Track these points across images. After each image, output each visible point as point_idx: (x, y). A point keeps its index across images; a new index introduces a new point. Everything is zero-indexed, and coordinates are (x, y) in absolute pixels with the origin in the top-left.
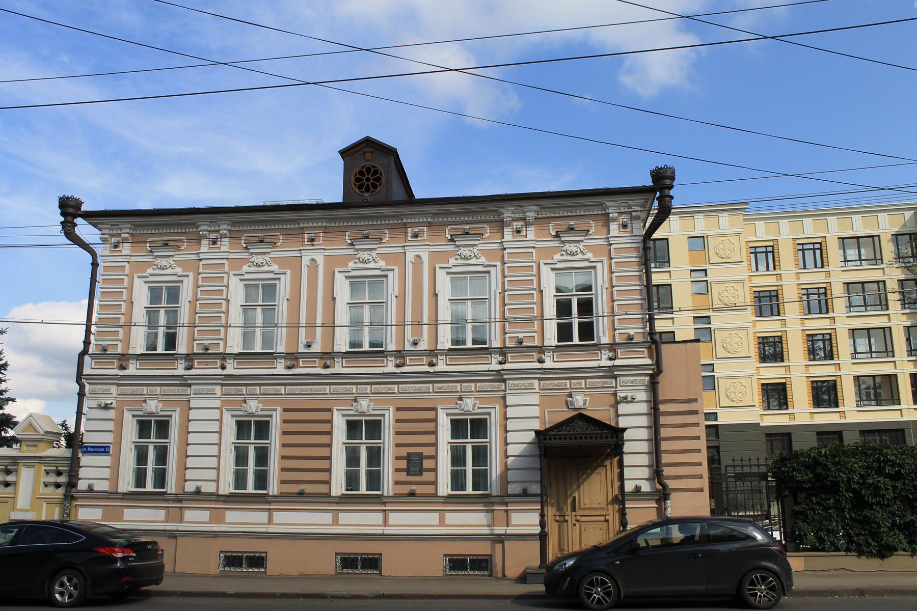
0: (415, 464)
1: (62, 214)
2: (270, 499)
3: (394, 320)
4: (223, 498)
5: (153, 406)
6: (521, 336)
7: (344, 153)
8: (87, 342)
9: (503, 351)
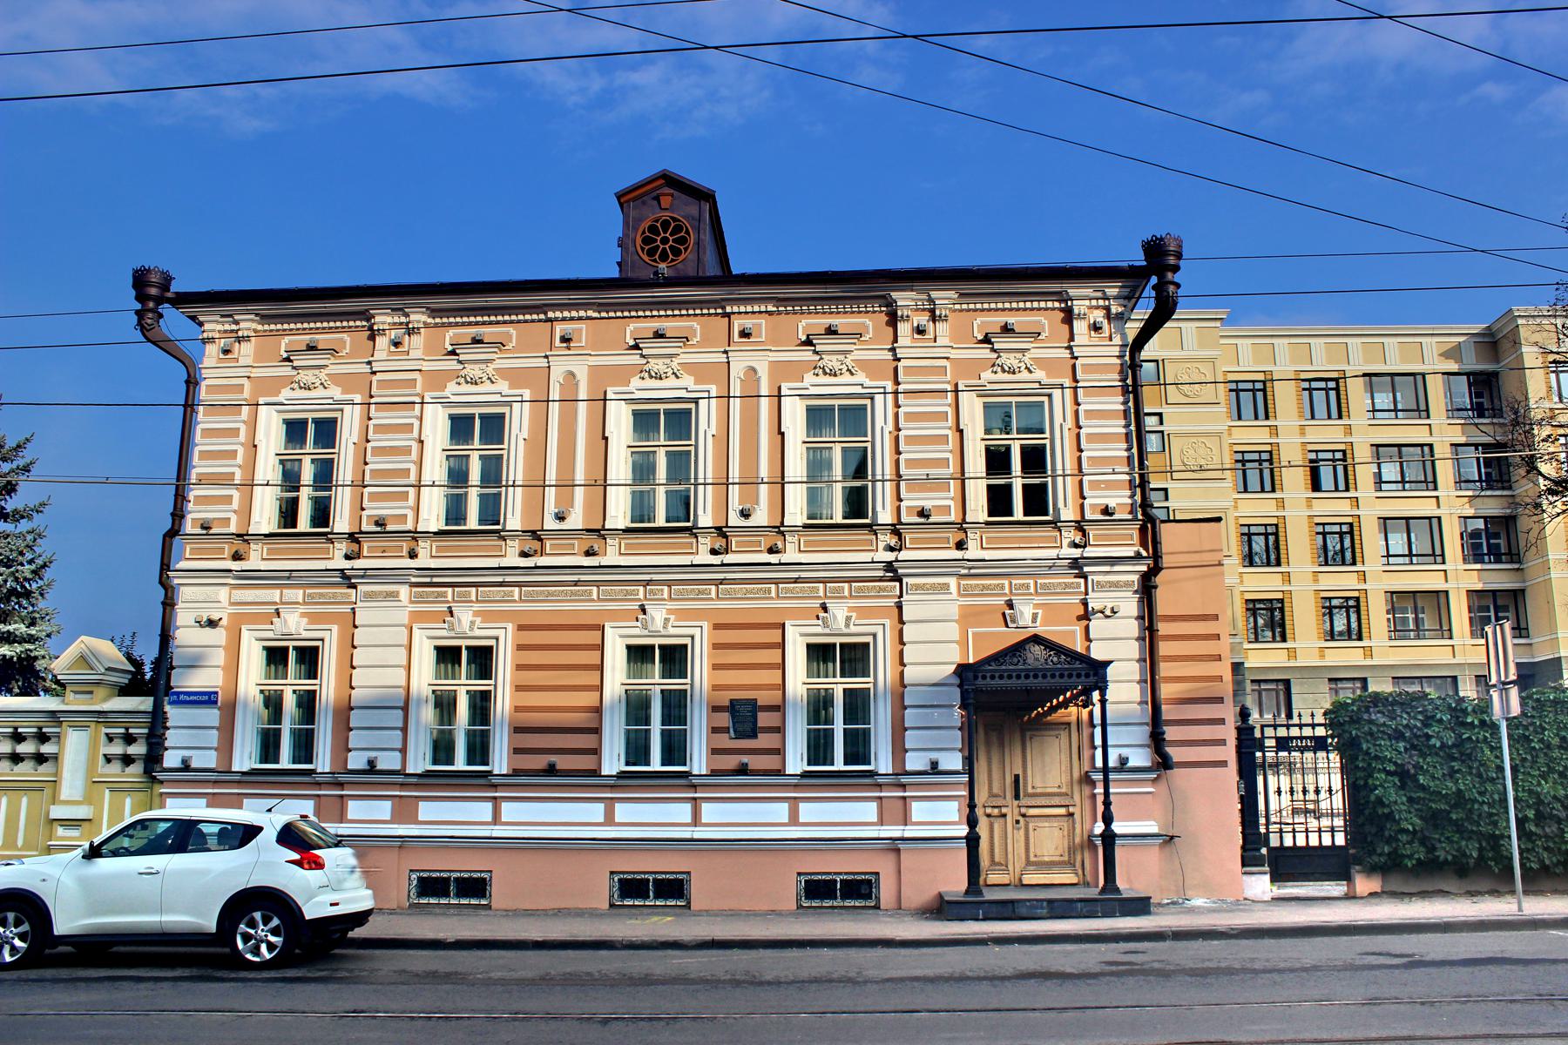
1: (138, 298)
2: (495, 781)
3: (710, 474)
4: (414, 780)
6: (928, 504)
7: (625, 198)
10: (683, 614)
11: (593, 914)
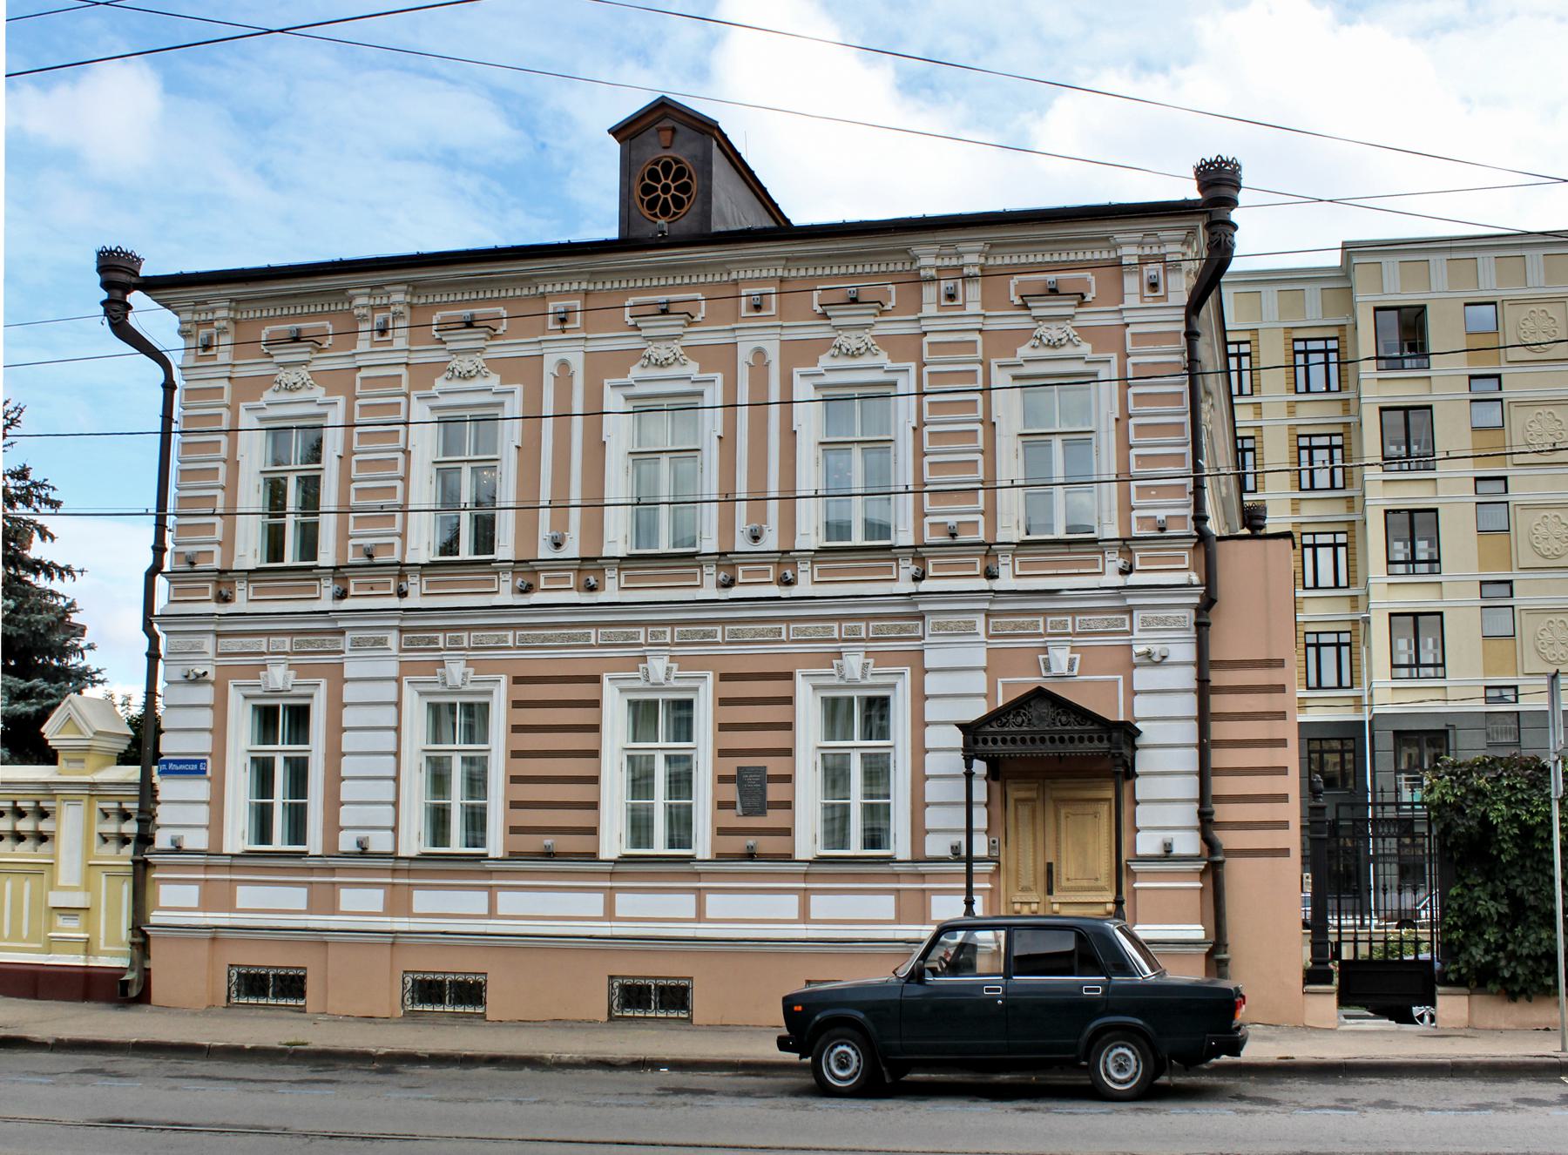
0: (755, 790)
1: (106, 285)
5: (279, 676)
7: (621, 132)
8: (159, 549)
9: (918, 553)
10: (880, 658)
11: (588, 1024)
